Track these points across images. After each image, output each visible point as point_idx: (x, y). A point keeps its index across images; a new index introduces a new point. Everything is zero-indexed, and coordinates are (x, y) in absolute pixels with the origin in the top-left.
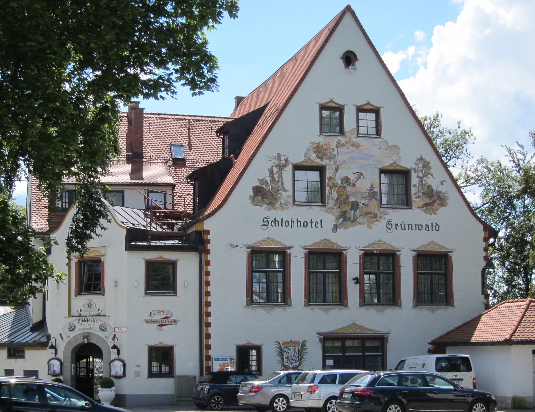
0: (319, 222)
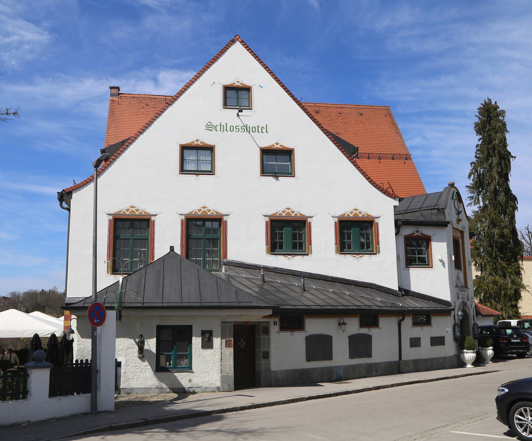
0: (265, 127)
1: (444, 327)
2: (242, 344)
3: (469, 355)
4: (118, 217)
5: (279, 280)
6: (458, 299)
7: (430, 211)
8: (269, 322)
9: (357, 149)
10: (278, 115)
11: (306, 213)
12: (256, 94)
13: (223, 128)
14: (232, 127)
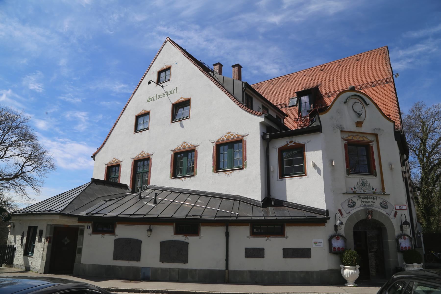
8: (84, 226)
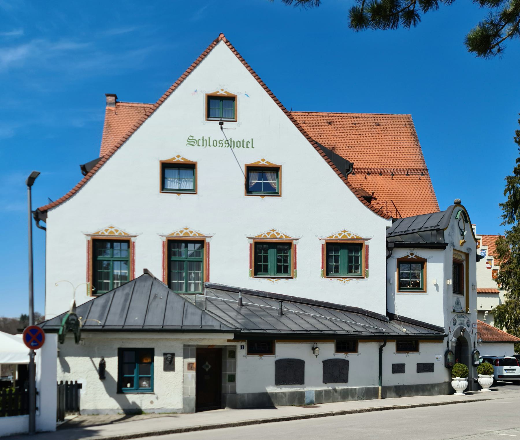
0: (251, 142)
1: (434, 353)
2: (207, 366)
3: (459, 383)
4: (97, 237)
5: (259, 304)
6: (455, 325)
7: (430, 232)
8: (235, 346)
9: (352, 165)
10: (265, 127)
11: (292, 235)
12: (241, 104)
13: (206, 142)
14: (215, 142)
